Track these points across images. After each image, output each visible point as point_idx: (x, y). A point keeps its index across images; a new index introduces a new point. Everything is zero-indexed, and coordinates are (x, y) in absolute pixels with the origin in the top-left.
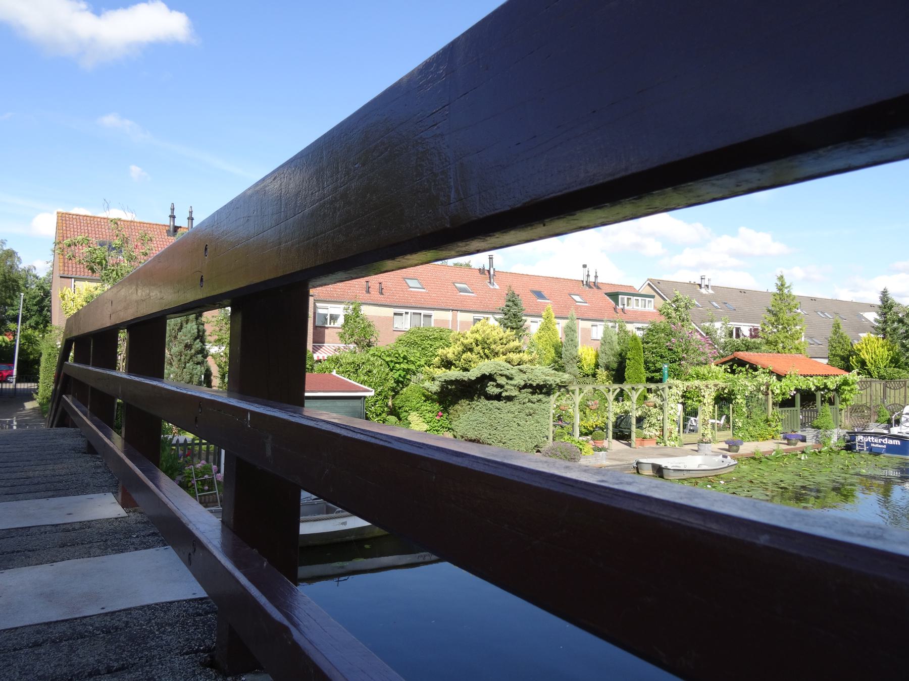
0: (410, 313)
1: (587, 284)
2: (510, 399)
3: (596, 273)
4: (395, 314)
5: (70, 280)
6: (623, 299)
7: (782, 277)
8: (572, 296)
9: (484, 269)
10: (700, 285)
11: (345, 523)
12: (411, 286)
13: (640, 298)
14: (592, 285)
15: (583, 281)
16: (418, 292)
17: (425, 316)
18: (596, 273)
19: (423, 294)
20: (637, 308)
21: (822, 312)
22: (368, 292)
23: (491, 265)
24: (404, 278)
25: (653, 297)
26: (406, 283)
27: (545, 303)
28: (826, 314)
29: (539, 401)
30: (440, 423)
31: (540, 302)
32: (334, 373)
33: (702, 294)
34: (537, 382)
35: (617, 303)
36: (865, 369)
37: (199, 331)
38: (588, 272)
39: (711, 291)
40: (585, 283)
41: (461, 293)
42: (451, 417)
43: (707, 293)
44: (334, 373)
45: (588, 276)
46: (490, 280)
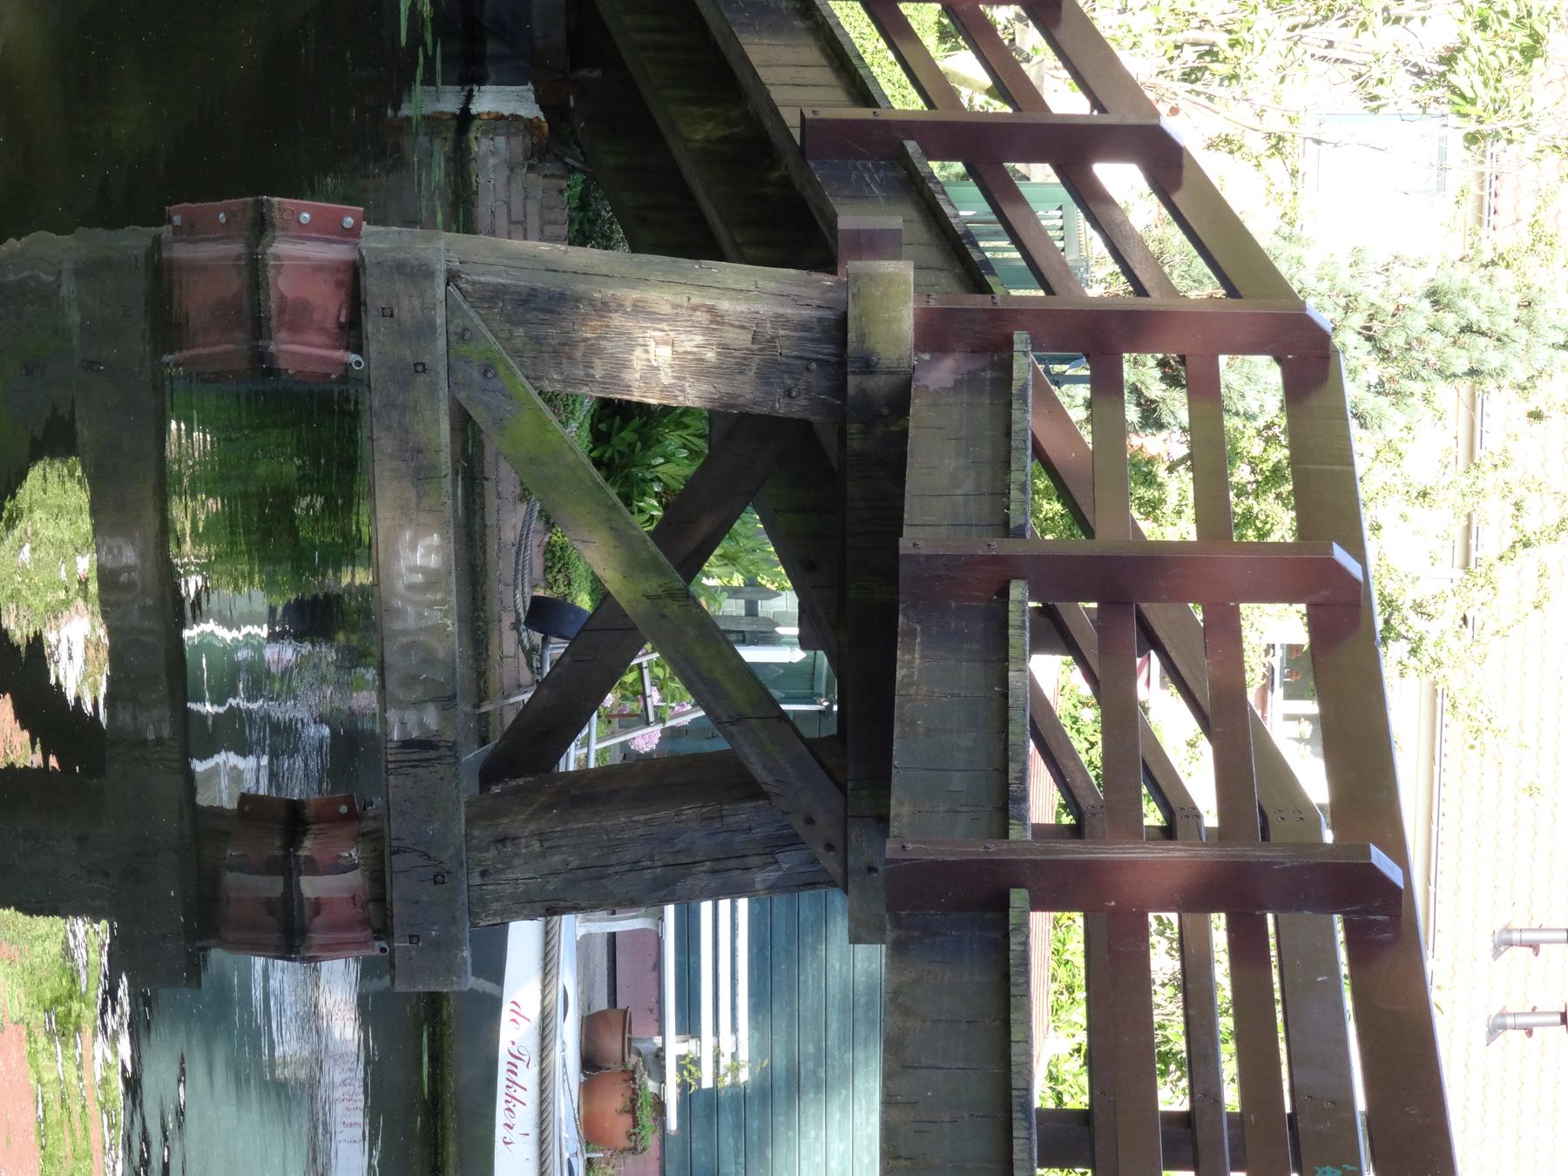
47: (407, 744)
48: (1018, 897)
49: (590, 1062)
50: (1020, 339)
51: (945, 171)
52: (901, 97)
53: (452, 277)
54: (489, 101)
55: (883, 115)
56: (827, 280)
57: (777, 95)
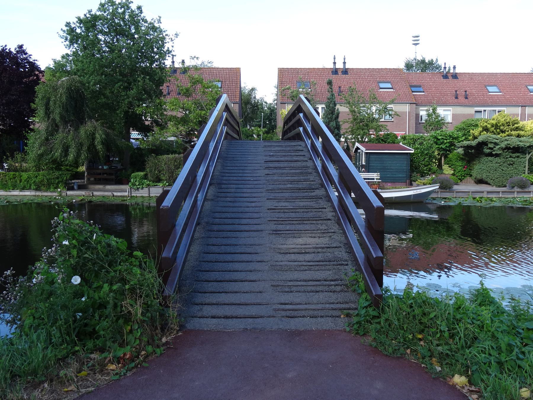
0: (487, 111)
2: (497, 155)
3: (345, 59)
4: (476, 112)
5: (284, 105)
16: (495, 95)
17: (499, 112)
18: (345, 59)
26: (487, 89)
29: (518, 157)
32: (401, 144)
34: (513, 145)
37: (336, 125)
44: (401, 144)
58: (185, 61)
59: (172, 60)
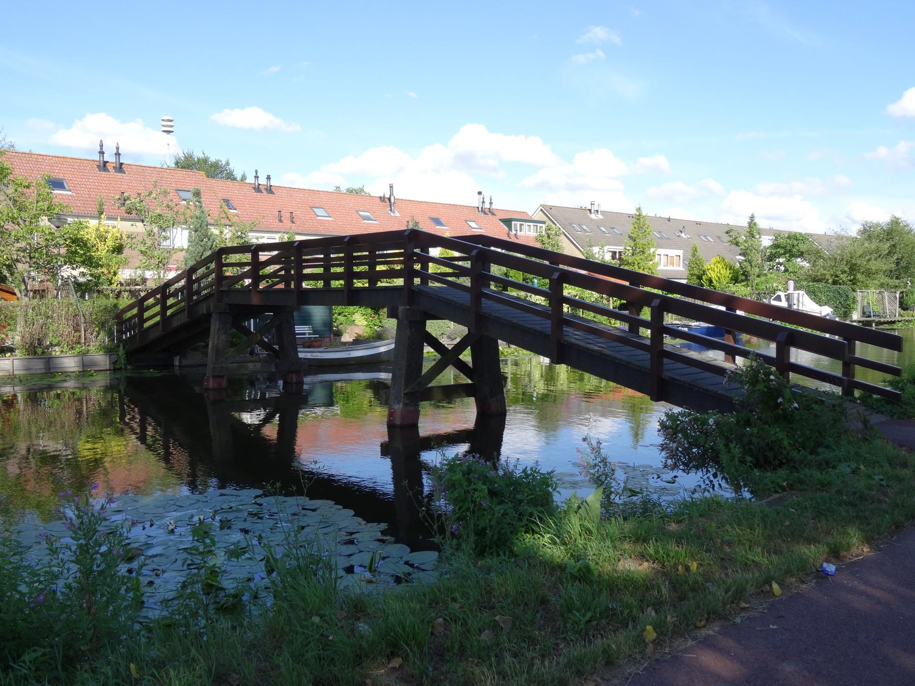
1: (482, 211)
3: (491, 199)
6: (516, 225)
7: (640, 208)
8: (468, 222)
9: (384, 197)
10: (590, 210)
11: (349, 354)
12: (318, 214)
13: (532, 224)
14: (487, 211)
15: (478, 208)
16: (326, 221)
18: (491, 199)
19: (331, 223)
20: (529, 233)
21: (705, 236)
22: (281, 221)
23: (391, 194)
24: (311, 207)
25: (544, 223)
26: (314, 211)
27: (443, 229)
28: (708, 237)
30: (373, 322)
31: (439, 229)
33: (591, 220)
35: (510, 229)
36: (712, 286)
38: (483, 198)
39: (600, 217)
40: (480, 209)
41: (365, 221)
42: (381, 317)
43: (597, 218)
45: (483, 202)
46: (391, 207)
47: (276, 369)
48: (301, 290)
49: (310, 347)
50: (221, 289)
51: (169, 312)
52: (158, 318)
53: (214, 364)
54: (177, 363)
55: (186, 307)
56: (213, 315)
57: (179, 323)
58: (726, 231)
59: (99, 150)
